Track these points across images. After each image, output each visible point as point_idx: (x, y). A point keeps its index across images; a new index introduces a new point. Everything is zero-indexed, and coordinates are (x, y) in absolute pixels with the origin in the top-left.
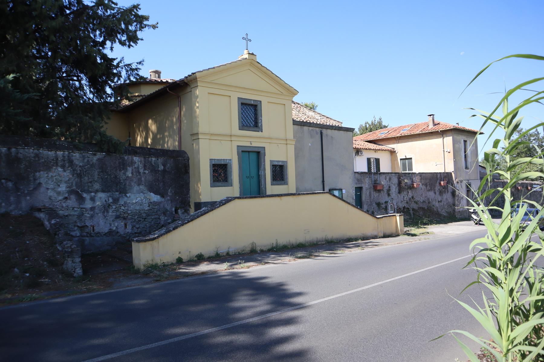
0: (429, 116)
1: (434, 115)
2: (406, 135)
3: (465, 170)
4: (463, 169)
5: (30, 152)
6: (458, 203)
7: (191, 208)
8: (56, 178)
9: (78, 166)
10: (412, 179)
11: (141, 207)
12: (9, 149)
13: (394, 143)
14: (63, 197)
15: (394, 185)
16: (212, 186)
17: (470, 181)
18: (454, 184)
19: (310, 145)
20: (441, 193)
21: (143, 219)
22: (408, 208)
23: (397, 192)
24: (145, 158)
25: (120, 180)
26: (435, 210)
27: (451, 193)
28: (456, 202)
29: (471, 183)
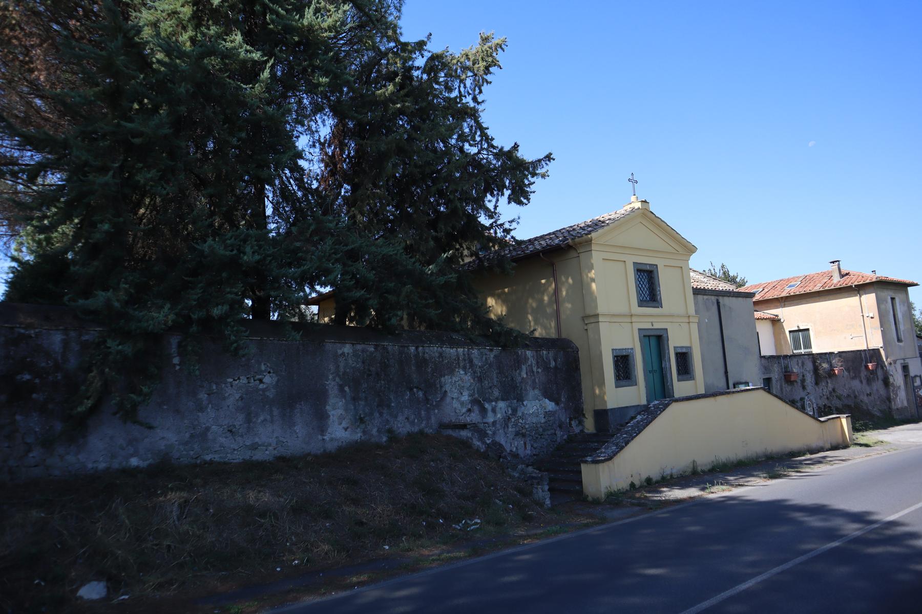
0: (831, 263)
1: (839, 261)
2: (798, 293)
3: (898, 343)
4: (895, 343)
5: (432, 351)
6: (894, 396)
7: (587, 418)
8: (458, 385)
9: (478, 367)
10: (831, 362)
11: (538, 419)
12: (417, 348)
13: (777, 307)
14: (466, 409)
15: (809, 372)
16: (617, 387)
17: (907, 361)
18: (885, 366)
19: (707, 321)
20: (869, 381)
21: (539, 435)
22: (829, 407)
23: (813, 383)
24: (537, 351)
25: (517, 384)
26: (865, 408)
27: (882, 380)
28: (892, 395)
29: (907, 363)
